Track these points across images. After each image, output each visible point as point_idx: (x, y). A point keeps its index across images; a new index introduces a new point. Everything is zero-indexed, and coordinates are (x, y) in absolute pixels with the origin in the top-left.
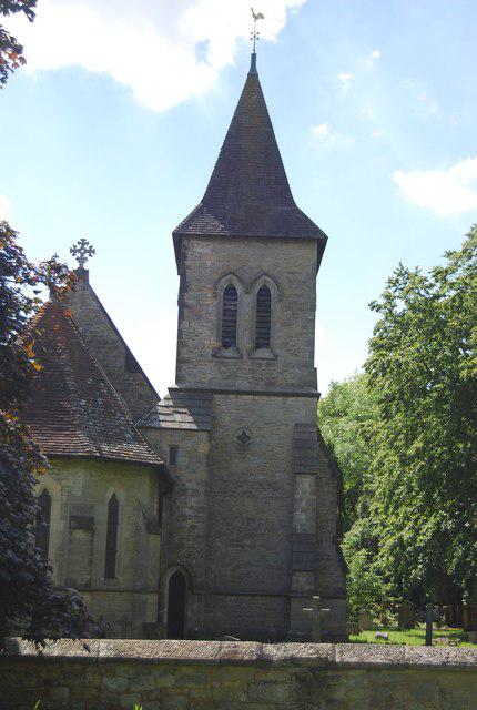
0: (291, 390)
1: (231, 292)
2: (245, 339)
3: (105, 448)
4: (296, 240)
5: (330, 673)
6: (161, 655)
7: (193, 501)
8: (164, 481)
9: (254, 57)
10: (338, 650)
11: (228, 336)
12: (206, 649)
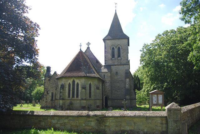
0: (124, 64)
1: (113, 48)
2: (116, 56)
3: (88, 75)
4: (124, 38)
5: (105, 119)
6: (64, 114)
7: (108, 84)
8: (103, 82)
9: (116, 10)
10: (107, 113)
11: (113, 56)
12: (75, 113)
